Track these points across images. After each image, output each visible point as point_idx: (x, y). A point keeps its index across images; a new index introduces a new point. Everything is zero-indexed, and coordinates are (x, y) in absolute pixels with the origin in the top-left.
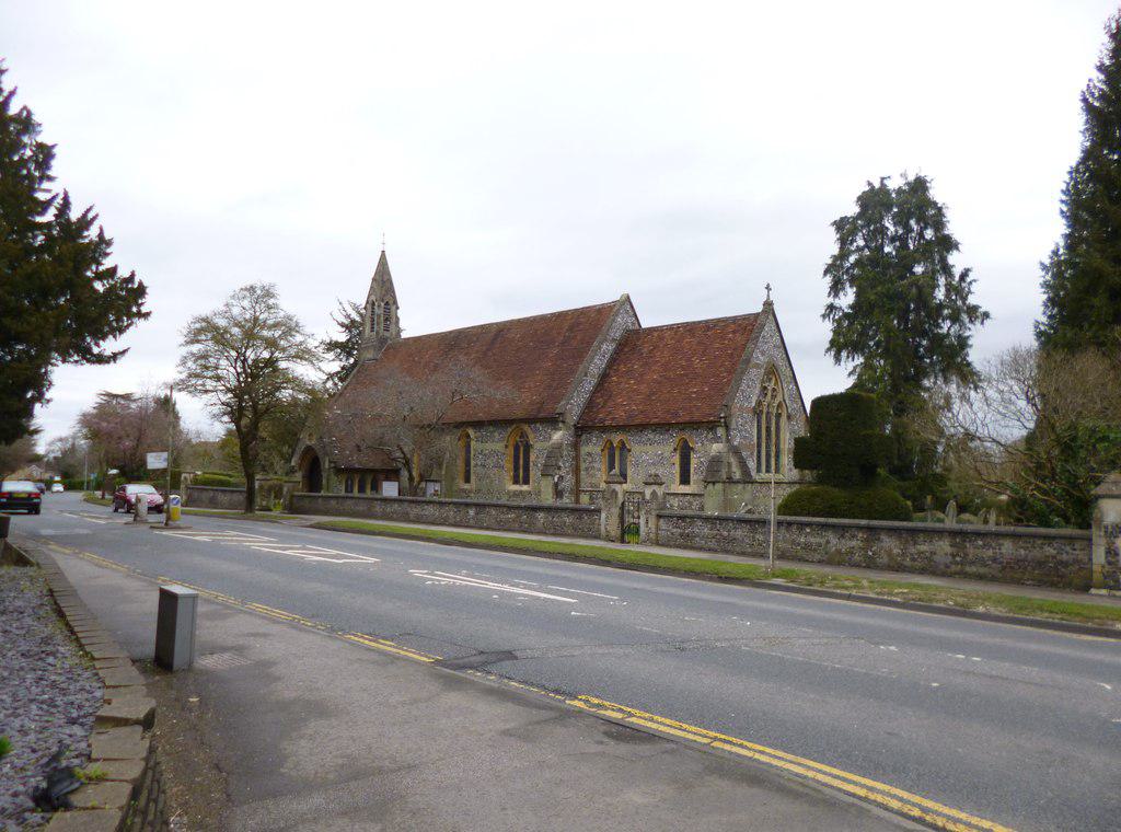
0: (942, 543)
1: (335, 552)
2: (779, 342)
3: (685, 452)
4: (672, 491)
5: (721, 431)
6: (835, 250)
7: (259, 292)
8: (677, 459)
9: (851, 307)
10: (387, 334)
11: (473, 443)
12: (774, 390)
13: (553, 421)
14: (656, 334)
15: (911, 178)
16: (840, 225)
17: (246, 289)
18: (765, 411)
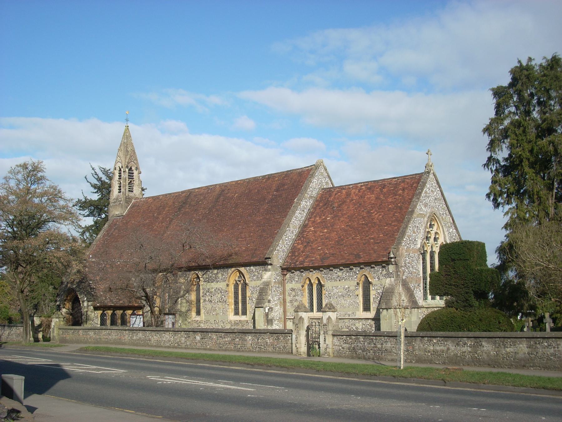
0: (521, 346)
1: (95, 367)
2: (440, 195)
3: (367, 285)
4: (357, 317)
5: (391, 268)
6: (492, 114)
7: (30, 168)
8: (360, 291)
9: (506, 160)
10: (131, 194)
11: (201, 283)
12: (436, 233)
13: (264, 263)
14: (344, 192)
15: (549, 57)
16: (498, 93)
17: (20, 166)
18: (429, 251)
